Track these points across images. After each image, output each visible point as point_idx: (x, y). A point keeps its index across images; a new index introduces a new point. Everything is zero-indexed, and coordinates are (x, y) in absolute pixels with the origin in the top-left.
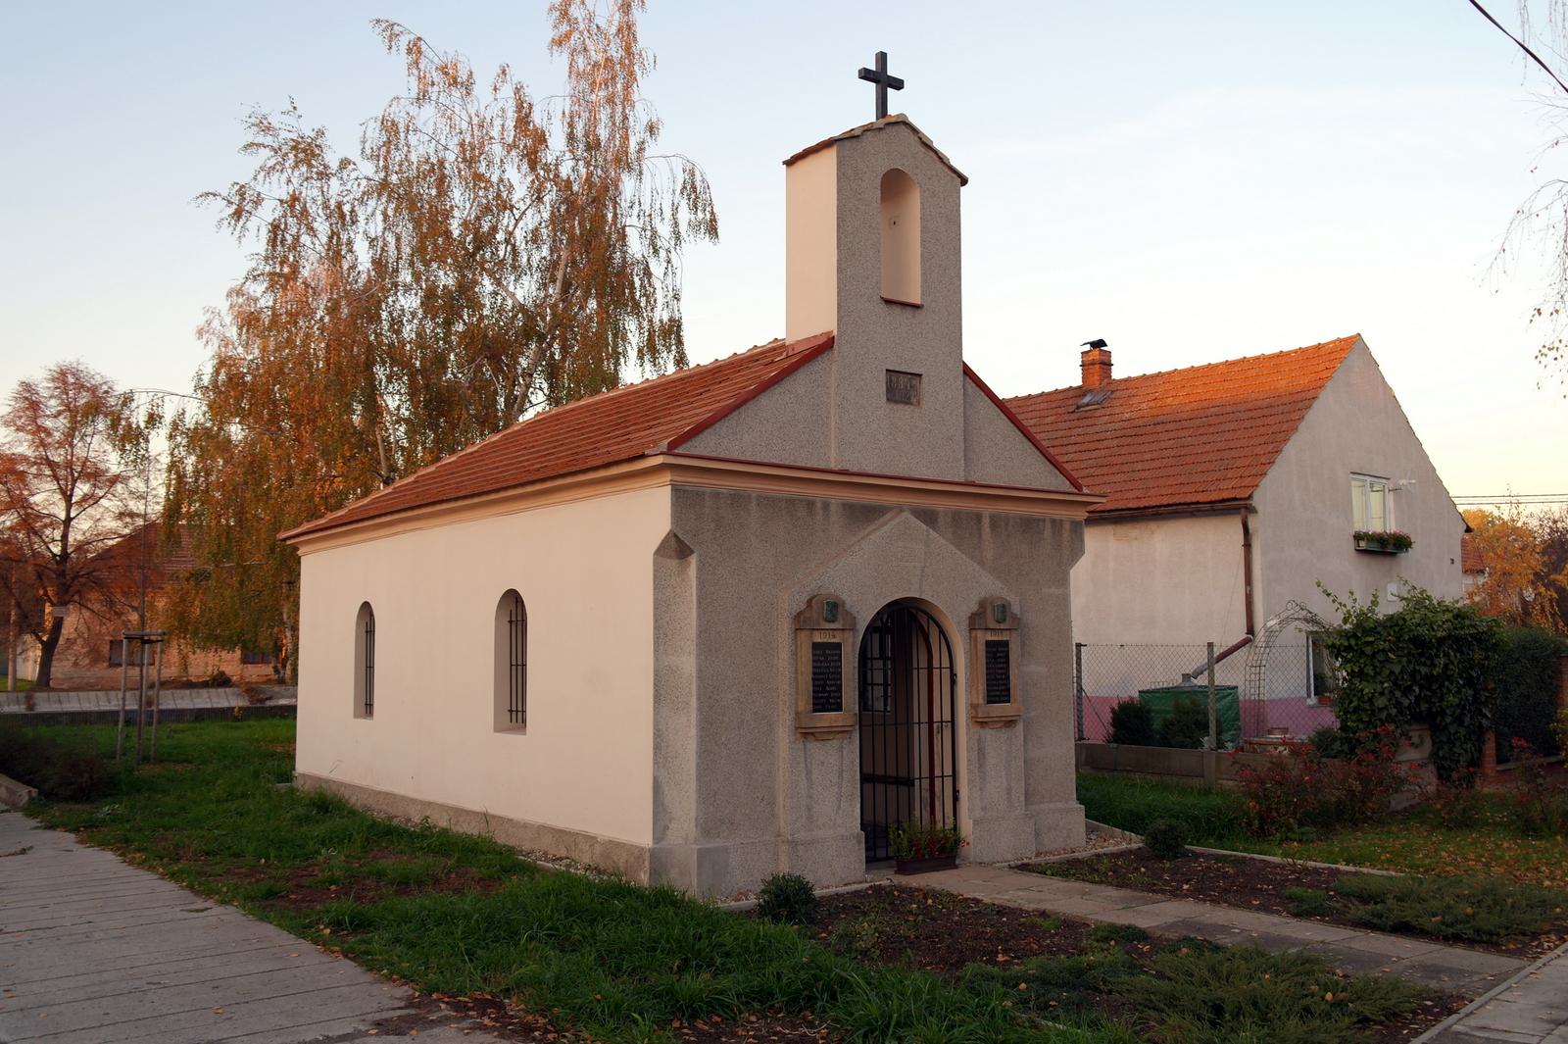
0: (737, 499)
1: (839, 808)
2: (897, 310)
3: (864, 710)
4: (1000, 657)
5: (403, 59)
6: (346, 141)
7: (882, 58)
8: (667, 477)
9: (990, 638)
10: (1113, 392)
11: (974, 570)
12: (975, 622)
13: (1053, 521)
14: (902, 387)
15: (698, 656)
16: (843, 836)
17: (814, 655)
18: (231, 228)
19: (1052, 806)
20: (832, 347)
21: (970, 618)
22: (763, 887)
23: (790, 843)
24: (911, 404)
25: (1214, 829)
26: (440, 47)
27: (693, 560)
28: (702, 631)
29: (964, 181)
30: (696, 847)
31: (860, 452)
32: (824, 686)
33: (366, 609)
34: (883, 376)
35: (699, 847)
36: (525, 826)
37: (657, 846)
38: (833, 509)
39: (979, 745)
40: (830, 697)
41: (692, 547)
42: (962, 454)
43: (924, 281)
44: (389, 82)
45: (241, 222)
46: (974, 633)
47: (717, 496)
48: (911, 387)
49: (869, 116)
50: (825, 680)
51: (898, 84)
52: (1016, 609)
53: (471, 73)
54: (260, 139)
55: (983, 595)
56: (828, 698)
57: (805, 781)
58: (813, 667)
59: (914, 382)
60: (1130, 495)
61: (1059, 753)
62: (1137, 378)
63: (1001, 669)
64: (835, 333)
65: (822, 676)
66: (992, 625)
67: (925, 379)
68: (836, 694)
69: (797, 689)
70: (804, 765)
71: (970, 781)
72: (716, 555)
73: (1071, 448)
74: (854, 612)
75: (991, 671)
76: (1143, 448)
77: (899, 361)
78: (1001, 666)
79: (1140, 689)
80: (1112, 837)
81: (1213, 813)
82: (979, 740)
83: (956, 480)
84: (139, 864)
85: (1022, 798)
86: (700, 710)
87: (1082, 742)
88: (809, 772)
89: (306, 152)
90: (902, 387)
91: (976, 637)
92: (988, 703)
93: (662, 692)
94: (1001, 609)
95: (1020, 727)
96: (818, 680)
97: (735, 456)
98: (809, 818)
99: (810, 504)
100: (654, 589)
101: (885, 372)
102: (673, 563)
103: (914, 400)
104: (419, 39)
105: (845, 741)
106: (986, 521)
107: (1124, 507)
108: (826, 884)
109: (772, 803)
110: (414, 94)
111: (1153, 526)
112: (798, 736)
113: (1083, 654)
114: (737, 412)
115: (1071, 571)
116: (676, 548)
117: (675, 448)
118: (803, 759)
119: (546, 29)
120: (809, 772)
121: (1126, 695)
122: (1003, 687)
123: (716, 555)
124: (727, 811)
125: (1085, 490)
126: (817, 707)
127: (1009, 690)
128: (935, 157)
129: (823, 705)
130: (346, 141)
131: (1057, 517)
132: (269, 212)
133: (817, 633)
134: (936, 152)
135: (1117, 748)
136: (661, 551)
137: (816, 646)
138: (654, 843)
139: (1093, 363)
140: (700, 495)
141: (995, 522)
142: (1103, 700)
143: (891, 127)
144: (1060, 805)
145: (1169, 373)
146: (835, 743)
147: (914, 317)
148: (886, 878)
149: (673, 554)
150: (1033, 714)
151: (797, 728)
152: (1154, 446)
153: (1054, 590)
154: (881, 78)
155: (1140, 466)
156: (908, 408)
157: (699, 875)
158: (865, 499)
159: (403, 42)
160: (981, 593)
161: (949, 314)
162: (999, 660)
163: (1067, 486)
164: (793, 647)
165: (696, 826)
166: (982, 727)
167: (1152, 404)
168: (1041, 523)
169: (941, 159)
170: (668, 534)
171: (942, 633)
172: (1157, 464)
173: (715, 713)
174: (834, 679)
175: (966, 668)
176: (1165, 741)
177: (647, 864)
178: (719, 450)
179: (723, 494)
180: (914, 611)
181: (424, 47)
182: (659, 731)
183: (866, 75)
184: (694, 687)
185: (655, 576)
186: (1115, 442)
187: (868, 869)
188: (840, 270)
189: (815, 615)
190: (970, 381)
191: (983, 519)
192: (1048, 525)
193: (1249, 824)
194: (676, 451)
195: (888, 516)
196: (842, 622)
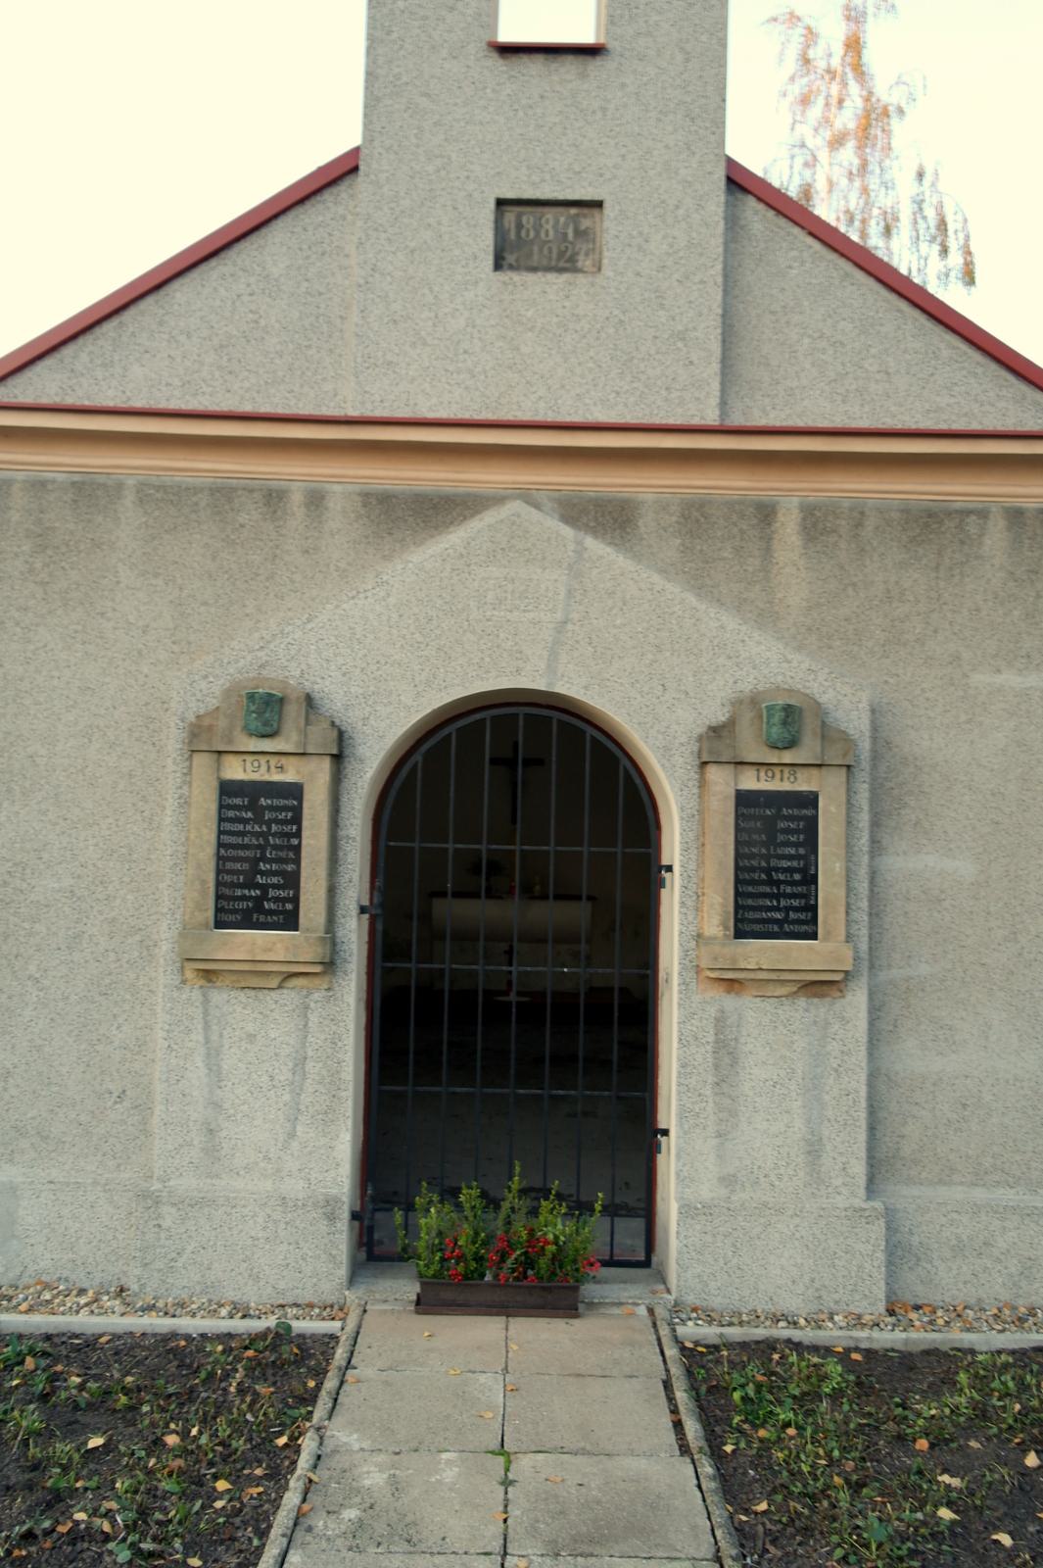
0: (88, 493)
1: (292, 1135)
12: (716, 746)
14: (538, 233)
19: (979, 1194)
24: (576, 270)
31: (413, 380)
38: (334, 505)
40: (264, 897)
42: (716, 367)
47: (39, 486)
48: (578, 233)
57: (203, 1071)
59: (585, 223)
63: (790, 857)
65: (247, 853)
68: (282, 894)
70: (201, 1039)
77: (535, 178)
82: (720, 1022)
85: (859, 1169)
88: (213, 1055)
95: (857, 1000)
98: (212, 1151)
99: (274, 498)
101: (492, 205)
103: (583, 262)
105: (316, 996)
106: (788, 525)
112: (189, 974)
120: (213, 1055)
123: (32, 602)
124: (35, 1112)
126: (232, 918)
133: (229, 760)
150: (924, 969)
158: (418, 472)
161: (687, 60)
173: (15, 914)
179: (54, 481)
190: (761, 207)
191: (780, 517)
196: (294, 737)
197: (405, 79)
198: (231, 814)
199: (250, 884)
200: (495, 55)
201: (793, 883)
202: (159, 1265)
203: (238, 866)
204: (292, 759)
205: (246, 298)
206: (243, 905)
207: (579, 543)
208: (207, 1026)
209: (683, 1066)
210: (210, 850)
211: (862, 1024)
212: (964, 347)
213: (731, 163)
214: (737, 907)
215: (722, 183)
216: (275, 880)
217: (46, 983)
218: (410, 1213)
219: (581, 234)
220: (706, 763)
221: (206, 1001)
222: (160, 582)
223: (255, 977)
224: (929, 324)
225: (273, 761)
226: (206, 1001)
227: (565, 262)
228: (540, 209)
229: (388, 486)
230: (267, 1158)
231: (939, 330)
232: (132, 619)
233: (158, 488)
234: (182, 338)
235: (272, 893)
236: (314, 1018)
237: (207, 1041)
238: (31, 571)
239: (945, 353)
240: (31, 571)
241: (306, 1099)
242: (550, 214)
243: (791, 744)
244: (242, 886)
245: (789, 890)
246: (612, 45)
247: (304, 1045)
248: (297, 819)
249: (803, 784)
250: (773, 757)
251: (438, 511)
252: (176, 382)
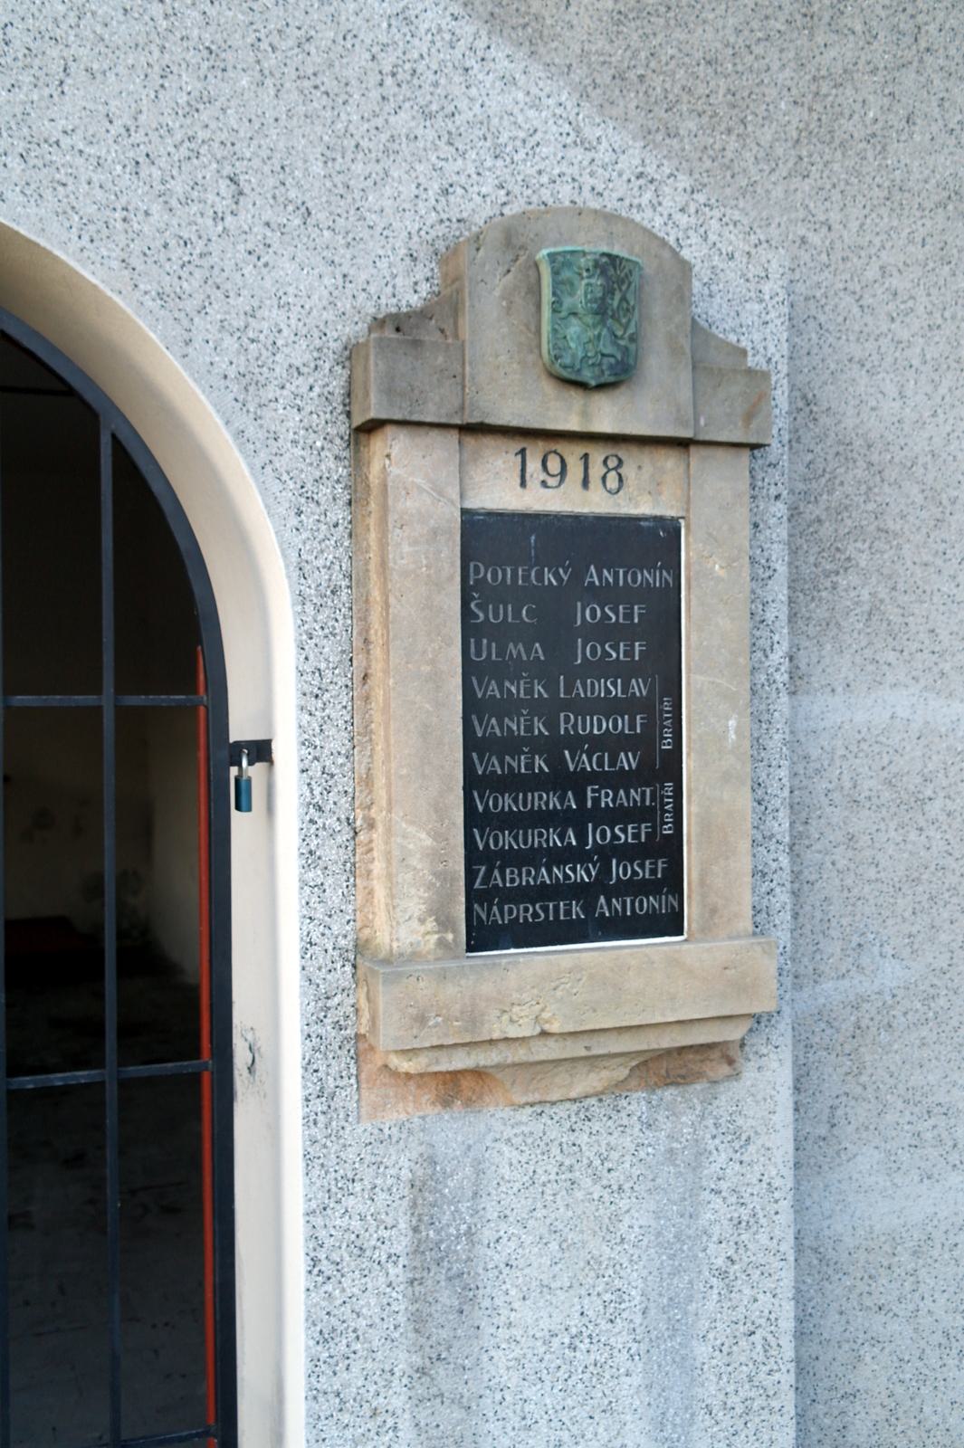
63: (611, 707)
82: (425, 1190)
84: (703, 930)
92: (481, 937)
94: (582, 292)
95: (768, 1079)
122: (512, 878)
127: (671, 849)
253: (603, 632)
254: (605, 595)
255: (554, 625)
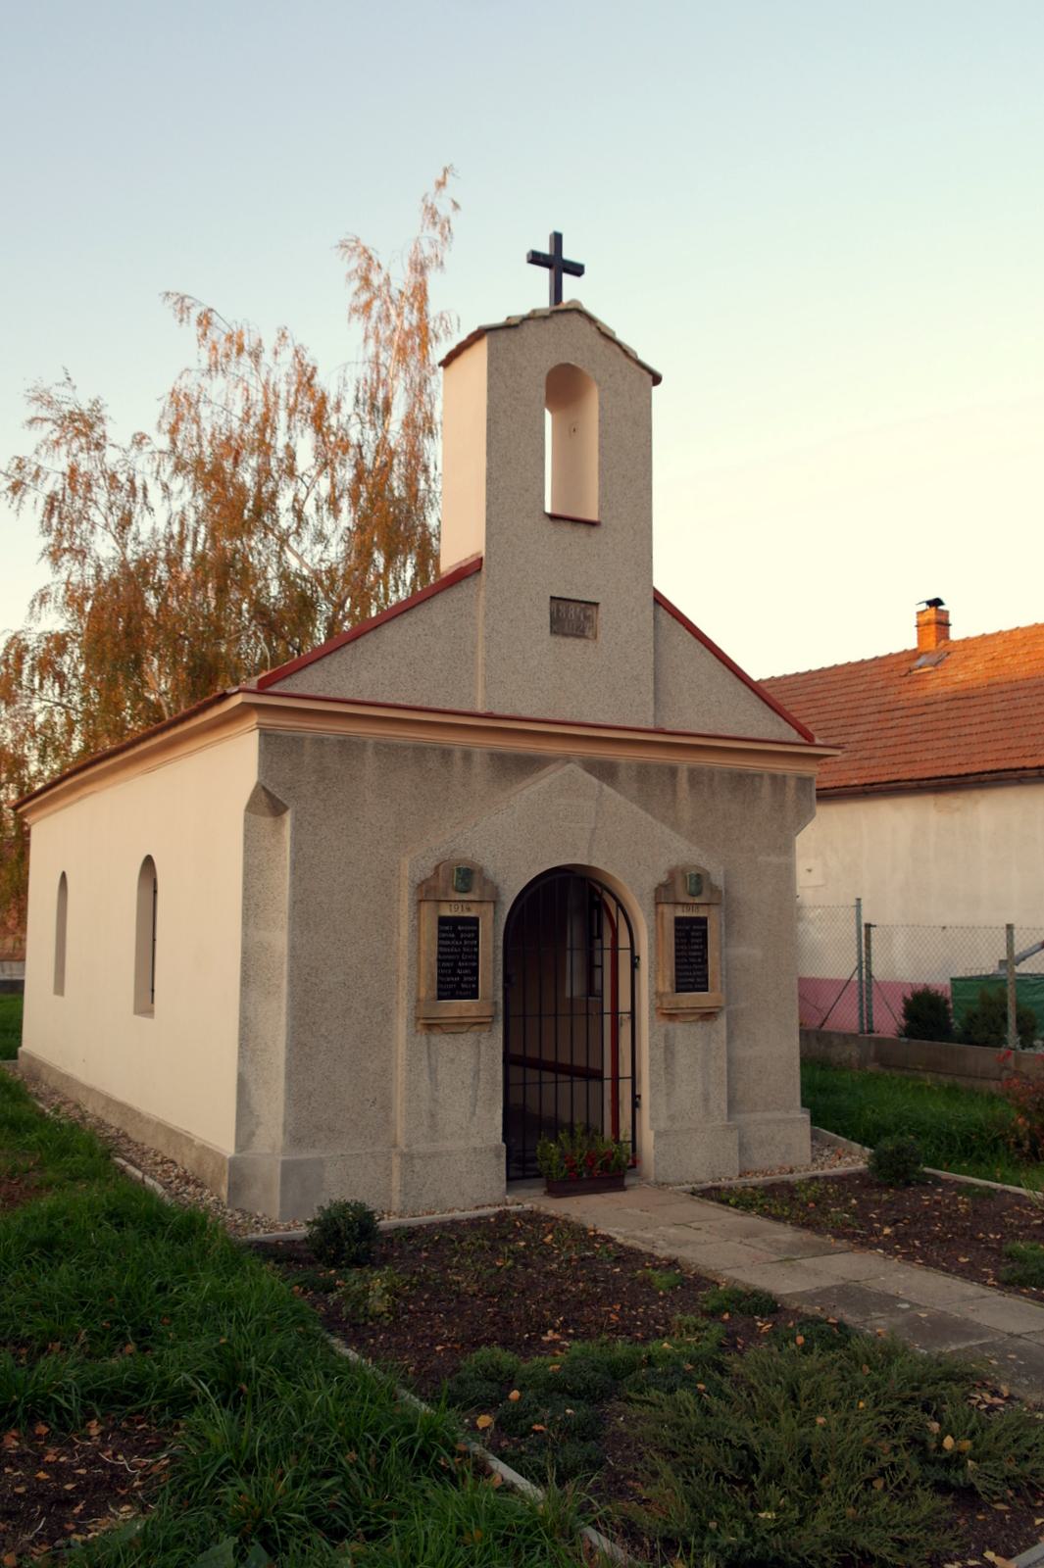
2: (566, 527)
3: (591, 995)
4: (695, 937)
5: (193, 330)
6: (133, 416)
7: (557, 239)
8: (254, 720)
9: (681, 913)
10: (949, 654)
11: (663, 833)
12: (663, 894)
13: (774, 778)
14: (571, 618)
15: (292, 931)
16: (475, 1148)
17: (440, 931)
18: (9, 501)
19: (768, 1115)
20: (480, 570)
21: (656, 889)
22: (317, 1217)
23: (402, 1155)
24: (586, 637)
25: (973, 1149)
26: (230, 315)
27: (288, 817)
28: (295, 903)
29: (657, 379)
30: (281, 1158)
32: (454, 968)
33: (64, 875)
34: (546, 605)
35: (286, 1158)
36: (149, 1122)
37: (239, 1155)
38: (477, 759)
39: (666, 1042)
40: (461, 981)
41: (285, 802)
42: (651, 695)
43: (603, 496)
44: (180, 355)
45: (18, 496)
46: (660, 907)
47: (319, 742)
49: (543, 302)
50: (456, 962)
51: (577, 270)
52: (718, 880)
53: (260, 341)
54: (44, 413)
55: (674, 863)
56: (458, 984)
58: (439, 946)
59: (589, 613)
60: (953, 761)
61: (777, 1052)
62: (976, 638)
63: (697, 950)
64: (483, 554)
65: (450, 957)
66: (684, 898)
67: (601, 607)
68: (470, 979)
69: (419, 972)
71: (653, 1085)
72: (317, 811)
73: (898, 714)
74: (498, 880)
75: (683, 953)
76: (972, 712)
77: (568, 587)
78: (696, 947)
79: (952, 976)
80: (850, 1154)
81: (973, 1129)
82: (666, 1036)
83: (643, 726)
85: (724, 1106)
86: (292, 995)
87: (873, 1035)
88: (433, 1072)
89: (83, 426)
90: (571, 618)
91: (663, 914)
92: (677, 991)
93: (252, 973)
95: (722, 1021)
96: (447, 961)
97: (349, 696)
98: (433, 1126)
99: (446, 754)
100: (245, 852)
101: (548, 599)
102: (266, 822)
103: (589, 633)
104: (211, 310)
107: (944, 774)
108: (450, 1206)
109: (387, 1107)
110: (205, 365)
111: (976, 794)
112: (419, 1027)
113: (873, 936)
114: (352, 645)
115: (798, 838)
116: (267, 802)
117: (270, 685)
118: (426, 1056)
119: (346, 293)
120: (433, 1072)
121: (920, 981)
122: (699, 973)
123: (317, 811)
125: (818, 741)
126: (445, 994)
127: (706, 976)
128: (618, 349)
129: (453, 991)
130: (133, 416)
131: (779, 773)
132: (53, 483)
134: (619, 345)
135: (908, 1043)
136: (252, 807)
137: (443, 921)
138: (237, 1152)
139: (928, 624)
140: (297, 742)
141: (695, 776)
142: (893, 986)
143: (562, 311)
144: (779, 1115)
145: (1011, 632)
146: (470, 1037)
147: (589, 536)
148: (533, 1200)
149: (266, 810)
151: (418, 1019)
152: (984, 709)
153: (774, 859)
154: (556, 263)
155: (967, 730)
156: (580, 643)
157: (284, 1193)
158: (518, 747)
159: (195, 313)
160: (674, 861)
162: (693, 941)
163: (793, 735)
164: (415, 922)
165: (284, 1133)
166: (670, 1020)
167: (989, 665)
168: (757, 779)
169: (626, 352)
170: (256, 787)
171: (620, 905)
172: (986, 727)
173: (313, 998)
174: (468, 960)
175: (650, 948)
176: (967, 1038)
177: (226, 1177)
178: (328, 689)
179: (328, 739)
180: (599, 888)
181: (215, 319)
182: (246, 1018)
183: (536, 259)
184: (285, 967)
185: (246, 836)
186: (945, 705)
187: (509, 1189)
188: (490, 480)
189: (442, 884)
190: (665, 612)
192: (767, 783)
193: (1019, 1144)
194: (270, 689)
195: (552, 767)
196: (478, 891)
197: (505, 525)
198: (444, 935)
199: (454, 974)
200: (548, 519)
201: (697, 963)
202: (413, 1193)
203: (448, 964)
204: (475, 904)
205: (423, 637)
206: (451, 986)
207: (601, 787)
208: (429, 1056)
209: (651, 1060)
210: (435, 957)
211: (724, 1033)
212: (750, 692)
213: (656, 593)
214: (677, 977)
215: (652, 600)
216: (466, 971)
217: (330, 1038)
218: (1004, 956)
219: (587, 618)
220: (420, 901)
221: (429, 1042)
222: (388, 801)
223: (458, 1026)
224: (736, 680)
225: (465, 905)
226: (429, 1042)
227: (579, 633)
228: (568, 603)
229: (503, 750)
230: (462, 1128)
231: (739, 682)
232: (373, 821)
233: (385, 746)
234: (390, 657)
235: (465, 979)
236: (483, 1048)
237: (430, 1065)
238: (317, 792)
239: (743, 694)
240: (317, 792)
241: (480, 1093)
242: (572, 605)
243: (699, 893)
244: (449, 976)
245: (696, 967)
246: (603, 521)
247: (478, 1063)
248: (477, 937)
249: (701, 913)
250: (691, 900)
251: (528, 765)
252: (386, 682)
253: (695, 937)
254: (696, 930)
255: (688, 936)
